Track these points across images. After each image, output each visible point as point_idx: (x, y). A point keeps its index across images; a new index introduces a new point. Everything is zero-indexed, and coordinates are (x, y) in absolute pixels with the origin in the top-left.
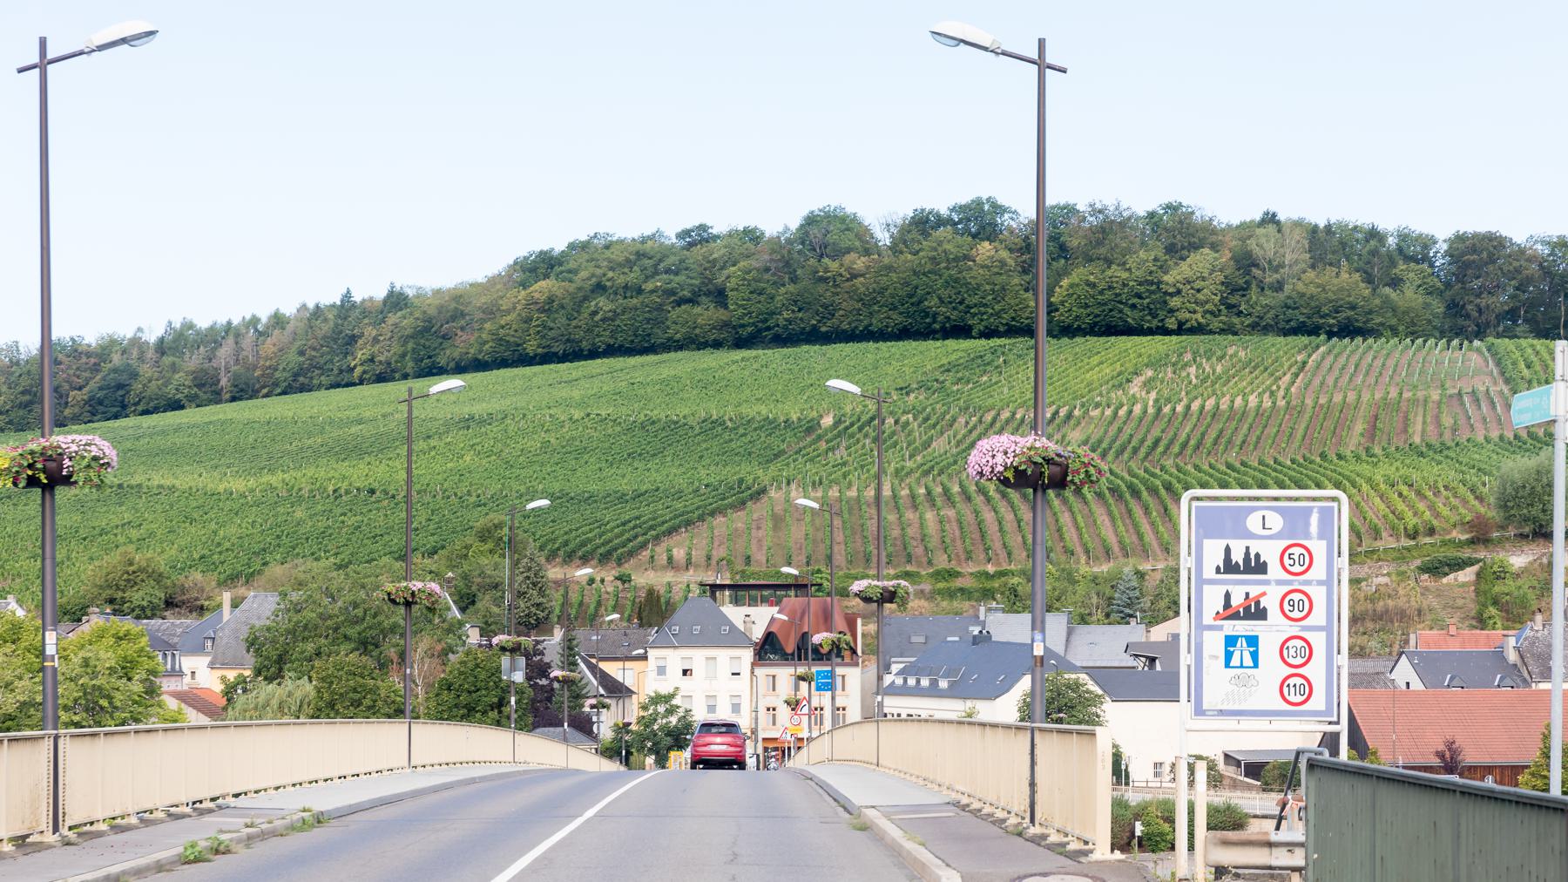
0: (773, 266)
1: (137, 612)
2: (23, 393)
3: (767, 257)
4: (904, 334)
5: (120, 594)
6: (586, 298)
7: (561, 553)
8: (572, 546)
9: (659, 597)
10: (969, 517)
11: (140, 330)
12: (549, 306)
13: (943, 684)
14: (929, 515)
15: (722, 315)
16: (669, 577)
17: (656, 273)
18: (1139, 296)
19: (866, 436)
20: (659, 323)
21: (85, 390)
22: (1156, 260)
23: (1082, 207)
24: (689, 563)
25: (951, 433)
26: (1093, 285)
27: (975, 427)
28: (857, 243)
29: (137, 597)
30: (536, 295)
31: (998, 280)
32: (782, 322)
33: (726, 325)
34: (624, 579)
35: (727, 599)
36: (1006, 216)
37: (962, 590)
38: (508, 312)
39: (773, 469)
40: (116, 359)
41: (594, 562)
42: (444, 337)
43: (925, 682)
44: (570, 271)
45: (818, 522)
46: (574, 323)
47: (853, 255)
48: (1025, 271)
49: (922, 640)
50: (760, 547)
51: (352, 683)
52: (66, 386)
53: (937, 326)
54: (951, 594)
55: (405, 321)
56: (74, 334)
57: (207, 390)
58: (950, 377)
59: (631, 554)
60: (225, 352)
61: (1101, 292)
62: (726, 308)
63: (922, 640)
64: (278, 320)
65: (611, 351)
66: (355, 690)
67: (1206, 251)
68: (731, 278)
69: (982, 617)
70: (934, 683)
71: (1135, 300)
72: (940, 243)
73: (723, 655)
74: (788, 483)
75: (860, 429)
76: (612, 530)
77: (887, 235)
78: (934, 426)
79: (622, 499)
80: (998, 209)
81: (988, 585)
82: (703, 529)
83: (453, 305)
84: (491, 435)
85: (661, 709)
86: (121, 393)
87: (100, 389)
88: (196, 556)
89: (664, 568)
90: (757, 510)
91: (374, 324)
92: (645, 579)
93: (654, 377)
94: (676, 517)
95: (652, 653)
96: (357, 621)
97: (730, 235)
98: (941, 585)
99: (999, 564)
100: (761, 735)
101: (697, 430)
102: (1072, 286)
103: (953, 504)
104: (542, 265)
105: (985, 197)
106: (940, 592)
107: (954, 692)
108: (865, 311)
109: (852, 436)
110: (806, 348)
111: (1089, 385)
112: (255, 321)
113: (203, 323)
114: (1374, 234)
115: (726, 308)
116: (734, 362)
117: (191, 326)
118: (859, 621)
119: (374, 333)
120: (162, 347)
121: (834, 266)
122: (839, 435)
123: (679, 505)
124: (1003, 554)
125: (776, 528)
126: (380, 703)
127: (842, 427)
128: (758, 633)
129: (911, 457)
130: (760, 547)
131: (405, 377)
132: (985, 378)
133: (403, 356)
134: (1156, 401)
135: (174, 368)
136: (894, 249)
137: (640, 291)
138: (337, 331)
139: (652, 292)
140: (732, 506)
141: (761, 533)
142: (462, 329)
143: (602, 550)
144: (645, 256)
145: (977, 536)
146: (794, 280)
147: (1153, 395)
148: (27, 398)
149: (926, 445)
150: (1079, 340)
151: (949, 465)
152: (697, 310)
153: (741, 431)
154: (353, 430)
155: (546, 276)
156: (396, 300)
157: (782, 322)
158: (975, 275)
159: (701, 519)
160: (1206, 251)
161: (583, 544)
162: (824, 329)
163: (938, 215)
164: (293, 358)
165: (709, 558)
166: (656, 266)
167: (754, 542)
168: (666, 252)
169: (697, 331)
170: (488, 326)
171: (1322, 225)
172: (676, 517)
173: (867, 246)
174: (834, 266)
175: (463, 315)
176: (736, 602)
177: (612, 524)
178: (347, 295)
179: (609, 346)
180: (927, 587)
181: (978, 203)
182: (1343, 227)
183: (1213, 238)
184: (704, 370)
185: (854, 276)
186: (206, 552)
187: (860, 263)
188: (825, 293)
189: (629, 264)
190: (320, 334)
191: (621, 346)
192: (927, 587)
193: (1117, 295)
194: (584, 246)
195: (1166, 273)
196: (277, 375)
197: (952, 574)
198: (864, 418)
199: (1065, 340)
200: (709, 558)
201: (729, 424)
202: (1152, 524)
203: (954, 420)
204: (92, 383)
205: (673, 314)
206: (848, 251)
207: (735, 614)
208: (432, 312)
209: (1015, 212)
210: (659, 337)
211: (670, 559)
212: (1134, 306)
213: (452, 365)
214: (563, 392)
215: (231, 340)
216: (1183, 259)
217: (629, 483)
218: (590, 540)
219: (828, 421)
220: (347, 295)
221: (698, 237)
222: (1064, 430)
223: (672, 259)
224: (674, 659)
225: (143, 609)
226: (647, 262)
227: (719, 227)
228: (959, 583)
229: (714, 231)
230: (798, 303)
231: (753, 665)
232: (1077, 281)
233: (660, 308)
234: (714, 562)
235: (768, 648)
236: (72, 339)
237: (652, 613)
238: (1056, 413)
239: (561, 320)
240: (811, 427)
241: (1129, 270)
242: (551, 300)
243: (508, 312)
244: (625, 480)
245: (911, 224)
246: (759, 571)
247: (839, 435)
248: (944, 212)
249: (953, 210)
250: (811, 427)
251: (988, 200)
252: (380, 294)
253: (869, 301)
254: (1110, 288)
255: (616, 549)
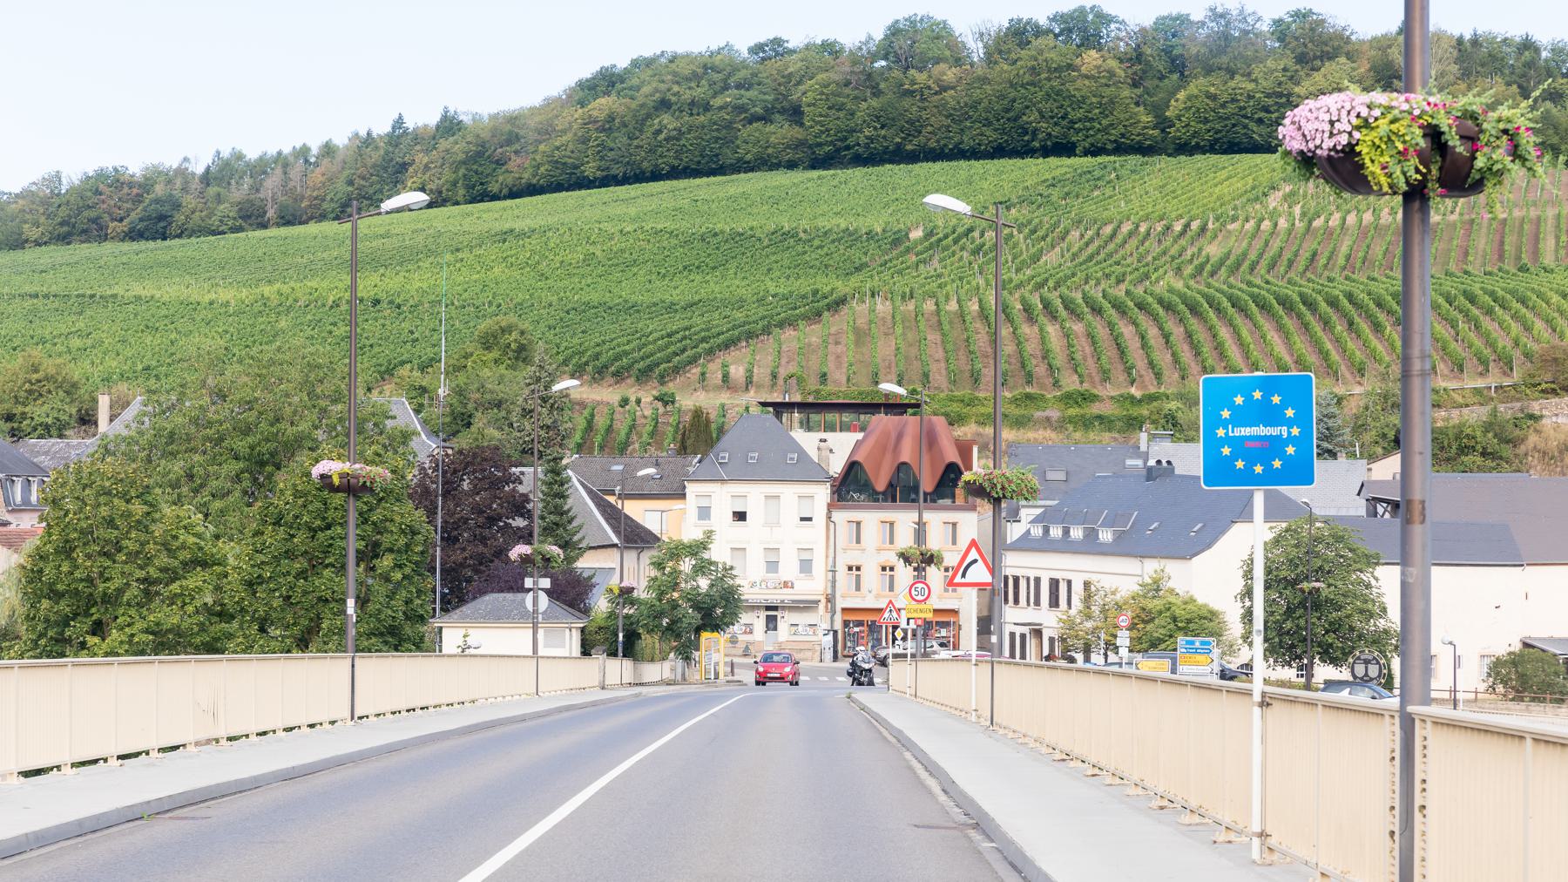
0: (853, 79)
1: (40, 431)
2: (61, 224)
3: (848, 69)
4: (998, 152)
5: (20, 409)
6: (649, 116)
7: (589, 369)
8: (603, 359)
9: (708, 422)
10: (1101, 332)
11: (186, 159)
12: (608, 125)
13: (1106, 536)
14: (1052, 330)
15: (797, 133)
16: (724, 398)
17: (726, 88)
18: (1266, 110)
19: (962, 249)
20: (729, 142)
21: (126, 222)
22: (1285, 70)
23: (1197, 16)
24: (749, 382)
25: (1064, 245)
26: (1213, 97)
27: (1091, 240)
28: (948, 53)
29: (40, 412)
30: (595, 113)
31: (1107, 92)
32: (862, 140)
33: (801, 144)
34: (666, 400)
35: (796, 424)
36: (1113, 26)
37: (1099, 417)
38: (564, 132)
39: (854, 281)
40: (159, 190)
41: (631, 381)
42: (497, 162)
43: (1077, 533)
44: (631, 89)
45: (910, 335)
46: (635, 142)
47: (943, 66)
48: (1135, 85)
49: (1062, 476)
50: (839, 366)
51: (104, 511)
52: (106, 217)
53: (1036, 144)
54: (1086, 423)
55: (457, 147)
56: (117, 164)
57: (252, 217)
58: (1055, 193)
59: (676, 370)
60: (272, 183)
61: (1223, 106)
62: (802, 125)
63: (1062, 476)
64: (328, 150)
65: (675, 173)
66: (110, 523)
67: (1343, 60)
68: (806, 93)
69: (1143, 448)
70: (1091, 534)
71: (1262, 115)
72: (1041, 52)
73: (789, 493)
74: (873, 295)
75: (956, 242)
76: (655, 341)
77: (980, 45)
78: (1044, 238)
79: (671, 308)
80: (1104, 19)
81: (1135, 411)
82: (770, 343)
83: (509, 127)
84: (528, 247)
85: (686, 565)
86: (162, 224)
87: (141, 220)
88: (140, 367)
89: (718, 388)
90: (834, 323)
91: (427, 152)
92: (688, 401)
93: (721, 195)
94: (734, 328)
95: (691, 489)
96: (247, 431)
97: (807, 47)
98: (1072, 411)
99: (1144, 387)
100: (841, 603)
101: (766, 242)
102: (1189, 98)
103: (1079, 317)
104: (607, 81)
105: (1088, 6)
106: (1071, 420)
107: (1124, 547)
108: (955, 128)
109: (946, 248)
110: (888, 166)
111: (1218, 198)
112: (303, 152)
113: (252, 154)
114: (1527, 45)
115: (802, 125)
116: (809, 180)
117: (239, 156)
118: (975, 449)
119: (426, 160)
120: (207, 178)
121: (921, 78)
122: (931, 247)
123: (739, 316)
124: (1149, 376)
125: (858, 343)
126: (151, 548)
127: (933, 239)
128: (837, 466)
129: (1018, 270)
130: (839, 366)
131: (457, 203)
132: (1096, 193)
133: (455, 184)
134: (1304, 214)
135: (219, 199)
136: (989, 59)
137: (707, 108)
138: (388, 159)
139: (721, 108)
140: (805, 317)
141: (840, 349)
142: (516, 152)
143: (641, 365)
144: (713, 71)
145: (1113, 353)
146: (877, 93)
147: (1297, 210)
148: (65, 229)
149: (1036, 258)
150: (1198, 157)
151: (1067, 277)
152: (770, 128)
153: (816, 243)
154: (374, 244)
155: (607, 93)
156: (449, 125)
157: (862, 140)
158: (1080, 87)
159: (766, 331)
160: (1343, 60)
161: (617, 358)
162: (909, 147)
163: (1037, 26)
164: (342, 188)
165: (774, 376)
166: (725, 80)
167: (831, 358)
168: (735, 67)
169: (770, 151)
170: (542, 147)
171: (1467, 37)
172: (734, 328)
173: (957, 56)
174: (921, 78)
175: (518, 138)
176: (807, 426)
177: (655, 335)
178: (399, 122)
179: (673, 168)
180: (1054, 414)
181: (1082, 11)
182: (1491, 40)
183: (1349, 47)
184: (777, 187)
185: (944, 89)
186: (154, 363)
187: (950, 74)
188: (911, 107)
189: (695, 77)
190: (370, 162)
191: (686, 168)
192: (1054, 414)
193: (1241, 108)
194: (649, 63)
195: (1298, 84)
196: (325, 205)
197: (1087, 398)
198: (960, 230)
199: (1183, 158)
200: (774, 376)
201: (802, 235)
202: (1337, 341)
203: (1067, 232)
204: (133, 214)
205: (744, 133)
206: (938, 61)
207: (808, 441)
208: (485, 135)
209: (1123, 22)
210: (729, 157)
211: (726, 377)
212: (1260, 121)
213: (505, 191)
214: (619, 210)
215: (279, 171)
216: (1318, 69)
217: (683, 292)
218: (626, 353)
219: (916, 234)
220: (399, 122)
221: (772, 50)
222: (1197, 244)
223: (743, 74)
224: (721, 497)
225: (47, 427)
226: (716, 77)
227: (795, 41)
228: (1095, 409)
229: (790, 46)
230: (881, 119)
231: (830, 507)
232: (1196, 92)
233: (729, 126)
234: (780, 382)
235: (851, 485)
236: (116, 170)
237: (699, 437)
238: (1187, 226)
239: (621, 140)
240: (898, 239)
241: (1255, 81)
242: (611, 118)
243: (564, 132)
244: (679, 291)
245: (1006, 35)
246: (839, 387)
247: (931, 247)
248: (1043, 22)
249: (1053, 19)
250: (898, 239)
251: (1092, 8)
252: (432, 119)
253: (960, 116)
254: (1233, 100)
255: (658, 365)
